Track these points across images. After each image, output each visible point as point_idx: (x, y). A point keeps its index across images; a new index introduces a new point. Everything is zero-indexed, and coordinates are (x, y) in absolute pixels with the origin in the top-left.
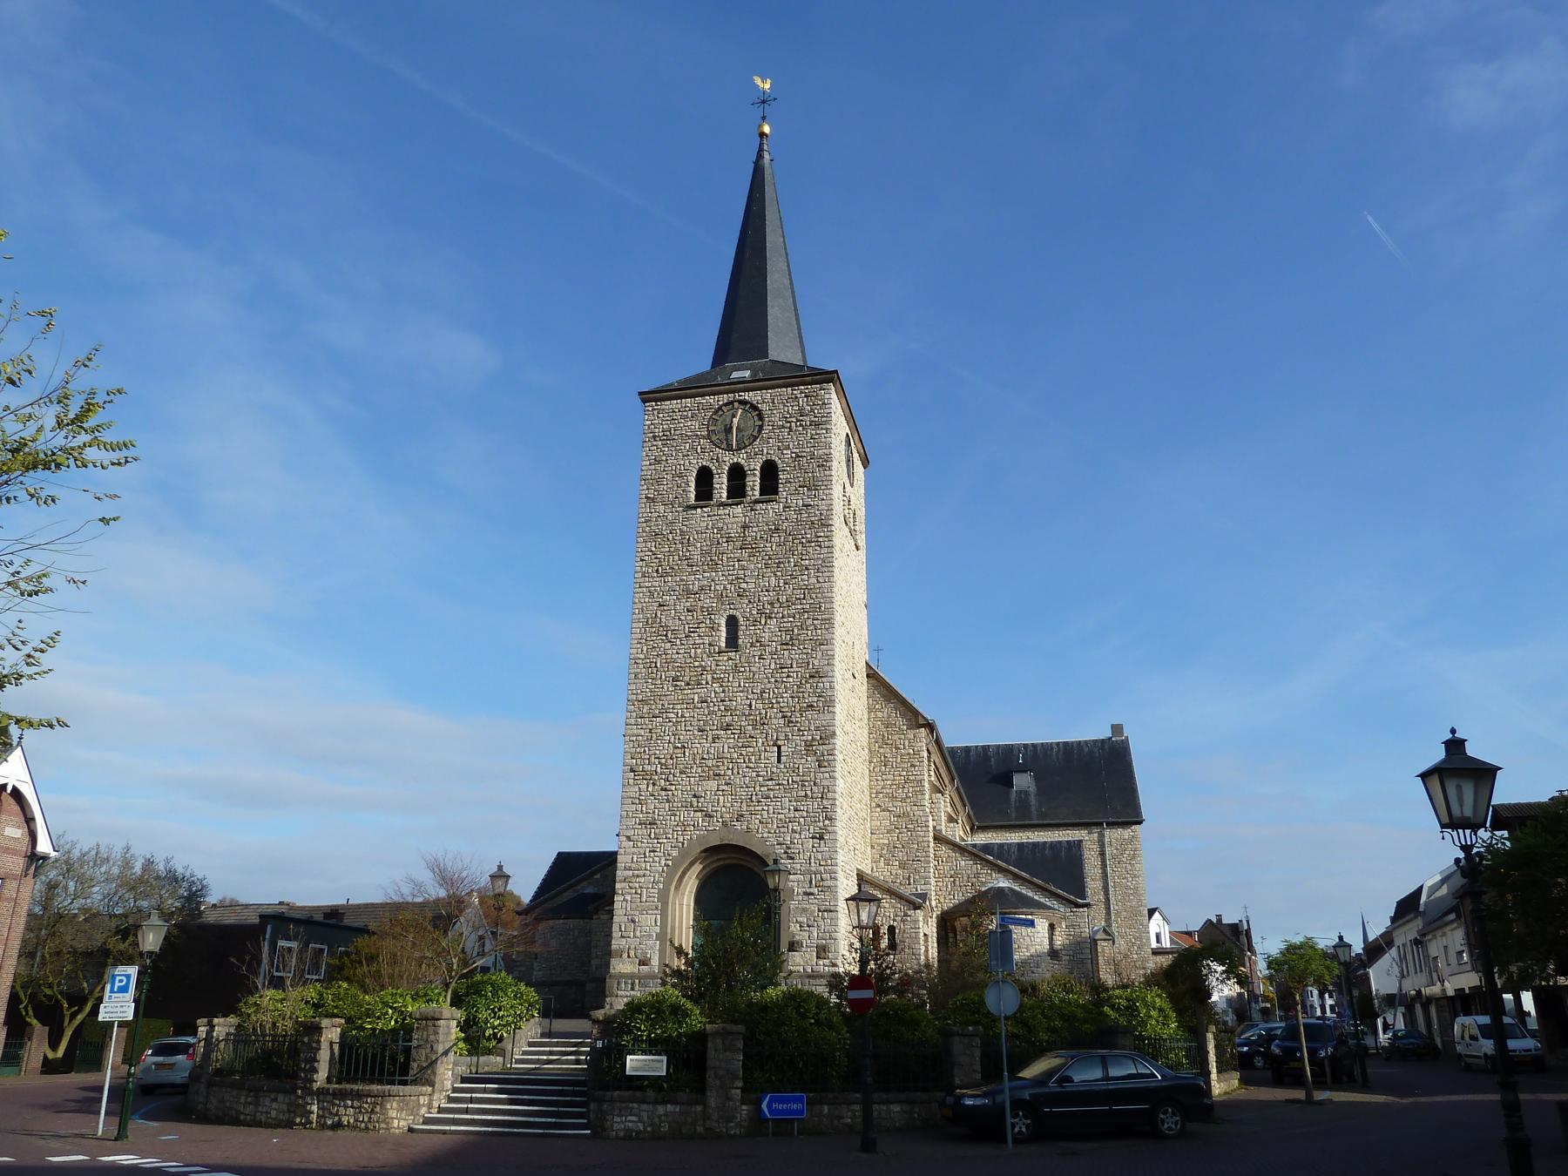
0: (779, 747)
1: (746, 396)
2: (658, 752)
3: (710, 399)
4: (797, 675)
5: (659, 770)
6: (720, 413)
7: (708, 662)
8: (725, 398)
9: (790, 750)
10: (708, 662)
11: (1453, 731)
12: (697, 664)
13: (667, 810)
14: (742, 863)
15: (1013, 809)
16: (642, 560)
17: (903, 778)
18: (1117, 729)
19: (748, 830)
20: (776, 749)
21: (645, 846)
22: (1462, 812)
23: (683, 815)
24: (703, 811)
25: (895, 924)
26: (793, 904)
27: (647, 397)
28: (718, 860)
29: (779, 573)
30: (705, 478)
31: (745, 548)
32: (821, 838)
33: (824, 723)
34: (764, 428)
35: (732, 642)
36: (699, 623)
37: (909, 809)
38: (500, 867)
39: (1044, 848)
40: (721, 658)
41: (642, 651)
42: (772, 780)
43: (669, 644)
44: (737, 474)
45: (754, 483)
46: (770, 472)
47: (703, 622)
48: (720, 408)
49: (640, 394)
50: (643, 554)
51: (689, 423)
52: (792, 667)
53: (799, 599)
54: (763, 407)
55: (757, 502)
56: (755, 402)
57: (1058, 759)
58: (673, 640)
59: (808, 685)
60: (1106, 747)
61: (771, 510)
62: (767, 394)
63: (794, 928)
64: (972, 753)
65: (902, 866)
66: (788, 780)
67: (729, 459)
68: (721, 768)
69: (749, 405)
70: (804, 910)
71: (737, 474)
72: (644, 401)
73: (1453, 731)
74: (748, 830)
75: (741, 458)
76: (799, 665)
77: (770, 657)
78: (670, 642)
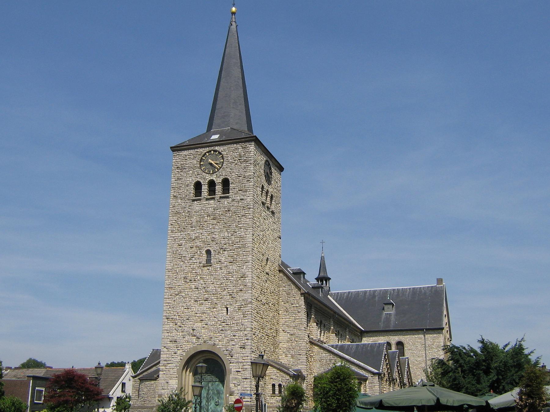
0: (227, 308)
1: (217, 148)
2: (177, 310)
3: (201, 150)
4: (235, 276)
5: (177, 318)
6: (206, 156)
7: (199, 271)
8: (207, 149)
9: (231, 309)
10: (199, 271)
11: (99, 362)
12: (194, 271)
13: (181, 335)
14: (213, 358)
15: (382, 323)
16: (172, 225)
17: (294, 317)
18: (440, 281)
19: (214, 344)
20: (226, 309)
21: (172, 352)
22: (161, 371)
23: (187, 338)
24: (196, 336)
25: (282, 383)
26: (231, 376)
27: (176, 149)
28: (203, 357)
29: (229, 230)
30: (198, 186)
31: (215, 219)
32: (244, 348)
33: (246, 298)
34: (224, 163)
35: (209, 261)
36: (195, 253)
37: (296, 331)
38: (99, 364)
39: (368, 346)
40: (204, 269)
41: (171, 266)
42: (224, 322)
43: (182, 263)
44: (212, 184)
45: (219, 188)
46: (226, 183)
47: (196, 253)
48: (205, 154)
49: (171, 148)
50: (171, 222)
51: (192, 161)
52: (233, 273)
53: (237, 242)
54: (223, 153)
55: (221, 198)
56: (220, 151)
57: (408, 296)
58: (184, 261)
59: (240, 281)
60: (433, 290)
61: (225, 202)
62: (225, 147)
63: (232, 385)
64: (368, 294)
65: (292, 357)
66: (231, 323)
67: (209, 178)
68: (203, 317)
69: (218, 152)
70: (236, 378)
71: (212, 184)
72: (173, 151)
73: (99, 362)
74: (214, 344)
75: (214, 177)
76: (236, 272)
77: (224, 268)
78: (183, 262)
